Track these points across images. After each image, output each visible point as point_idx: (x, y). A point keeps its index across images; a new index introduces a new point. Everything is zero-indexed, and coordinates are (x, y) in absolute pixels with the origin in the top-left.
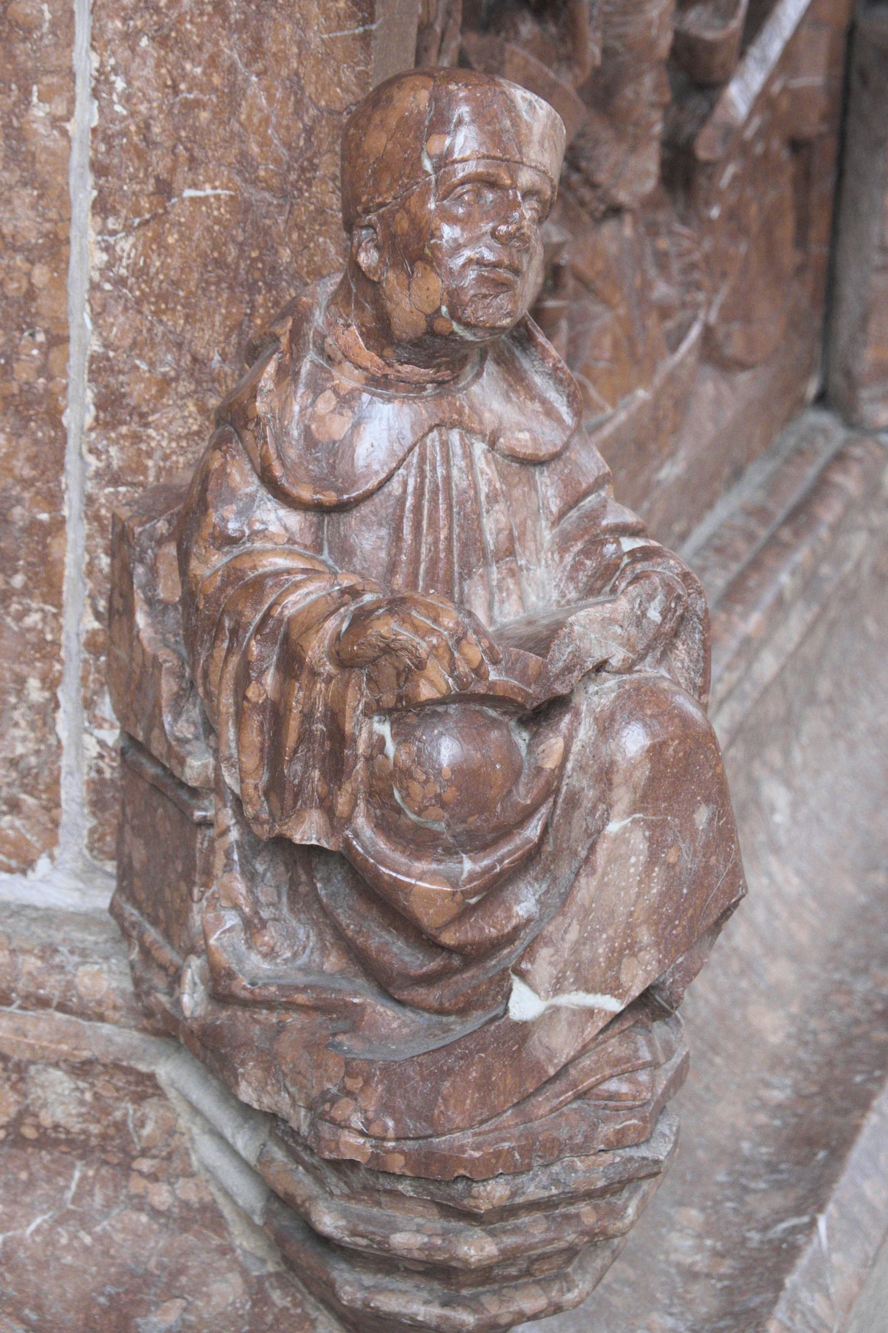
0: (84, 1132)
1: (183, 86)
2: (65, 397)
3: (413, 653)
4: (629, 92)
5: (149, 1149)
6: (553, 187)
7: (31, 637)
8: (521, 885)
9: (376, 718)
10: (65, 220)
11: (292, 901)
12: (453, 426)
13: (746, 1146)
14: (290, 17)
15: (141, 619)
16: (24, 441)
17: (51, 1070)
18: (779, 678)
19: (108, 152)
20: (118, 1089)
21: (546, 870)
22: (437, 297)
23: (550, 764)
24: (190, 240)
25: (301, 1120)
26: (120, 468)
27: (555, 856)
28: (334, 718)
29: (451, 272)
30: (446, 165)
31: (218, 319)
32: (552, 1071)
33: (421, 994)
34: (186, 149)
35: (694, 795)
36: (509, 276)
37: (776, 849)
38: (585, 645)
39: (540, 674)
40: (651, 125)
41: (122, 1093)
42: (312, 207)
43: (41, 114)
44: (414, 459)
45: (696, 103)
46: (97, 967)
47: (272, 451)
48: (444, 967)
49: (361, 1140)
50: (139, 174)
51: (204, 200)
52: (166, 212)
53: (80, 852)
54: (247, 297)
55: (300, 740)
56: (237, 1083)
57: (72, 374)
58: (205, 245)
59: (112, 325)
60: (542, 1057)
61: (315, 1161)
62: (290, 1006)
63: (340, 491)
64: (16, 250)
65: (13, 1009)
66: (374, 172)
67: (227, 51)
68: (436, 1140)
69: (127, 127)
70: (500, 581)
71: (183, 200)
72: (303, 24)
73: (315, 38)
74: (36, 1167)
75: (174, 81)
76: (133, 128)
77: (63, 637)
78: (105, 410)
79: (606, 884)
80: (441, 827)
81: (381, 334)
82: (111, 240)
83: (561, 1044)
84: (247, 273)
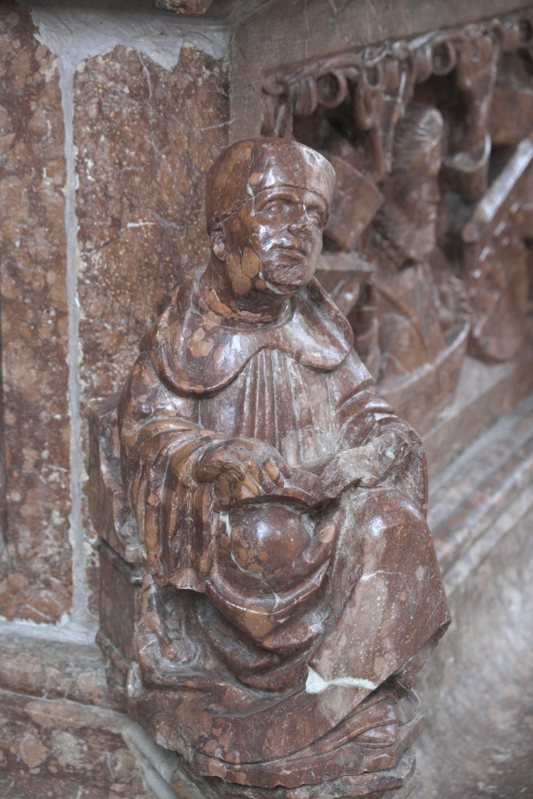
0: (83, 768)
1: (125, 163)
2: (67, 347)
3: (236, 469)
4: (414, 195)
5: (120, 778)
6: (327, 205)
7: (53, 487)
8: (314, 614)
9: (221, 513)
10: (63, 244)
11: (188, 629)
12: (273, 347)
13: (481, 785)
14: (183, 119)
15: (104, 468)
16: (45, 374)
17: (64, 733)
18: (514, 530)
19: (85, 203)
20: (101, 744)
21: (328, 605)
22: (256, 267)
23: (327, 540)
24: (132, 252)
25: (189, 754)
26: (98, 387)
27: (333, 597)
28: (197, 513)
29: (263, 253)
30: (260, 190)
31: (149, 297)
32: (333, 724)
33: (258, 680)
34: (128, 199)
35: (415, 560)
36: (299, 254)
37: (511, 624)
38: (346, 469)
39: (316, 485)
40: (428, 214)
41: (103, 746)
42: (199, 230)
43: (48, 184)
44: (250, 366)
45: (464, 211)
46: (89, 674)
47: (165, 361)
48: (269, 663)
49: (221, 765)
50: (102, 216)
51: (139, 229)
52: (118, 237)
53: (85, 611)
54: (164, 284)
55: (178, 527)
56: (155, 734)
57: (70, 333)
58: (140, 255)
59: (91, 304)
60: (328, 716)
61: (200, 779)
62: (185, 688)
63: (206, 385)
64: (37, 263)
65: (44, 698)
66: (221, 197)
67: (148, 141)
68: (264, 764)
69: (95, 188)
70: (304, 438)
71: (127, 229)
72: (190, 123)
73: (197, 131)
74: (57, 789)
75: (119, 160)
76: (98, 189)
77: (71, 486)
78: (89, 354)
79: (363, 613)
80: (259, 576)
81: (228, 293)
82: (89, 254)
83: (339, 708)
84: (164, 270)
